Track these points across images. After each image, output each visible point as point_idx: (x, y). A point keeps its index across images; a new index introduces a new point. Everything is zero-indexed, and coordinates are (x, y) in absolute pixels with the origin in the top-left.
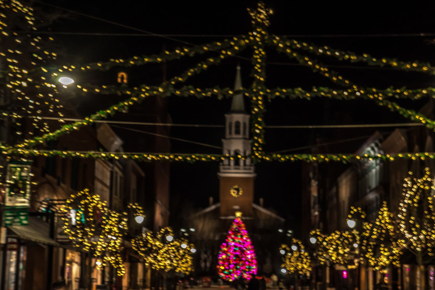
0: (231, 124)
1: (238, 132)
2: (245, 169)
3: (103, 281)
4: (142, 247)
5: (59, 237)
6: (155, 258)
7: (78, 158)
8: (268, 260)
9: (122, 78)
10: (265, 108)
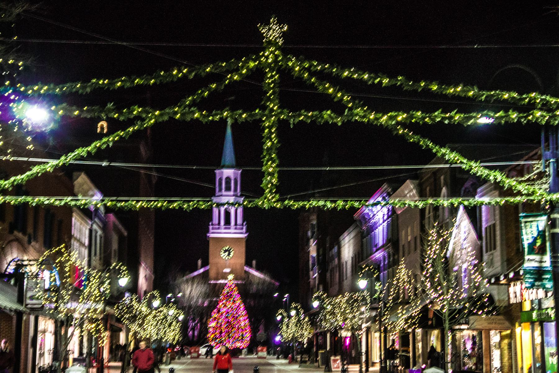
0: (221, 179)
1: (228, 189)
2: (236, 228)
3: (81, 353)
4: (126, 313)
5: (28, 301)
6: (140, 325)
7: (50, 206)
8: (262, 327)
9: (102, 128)
10: (278, 142)
